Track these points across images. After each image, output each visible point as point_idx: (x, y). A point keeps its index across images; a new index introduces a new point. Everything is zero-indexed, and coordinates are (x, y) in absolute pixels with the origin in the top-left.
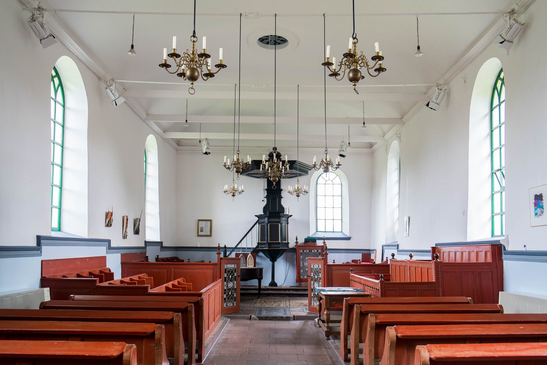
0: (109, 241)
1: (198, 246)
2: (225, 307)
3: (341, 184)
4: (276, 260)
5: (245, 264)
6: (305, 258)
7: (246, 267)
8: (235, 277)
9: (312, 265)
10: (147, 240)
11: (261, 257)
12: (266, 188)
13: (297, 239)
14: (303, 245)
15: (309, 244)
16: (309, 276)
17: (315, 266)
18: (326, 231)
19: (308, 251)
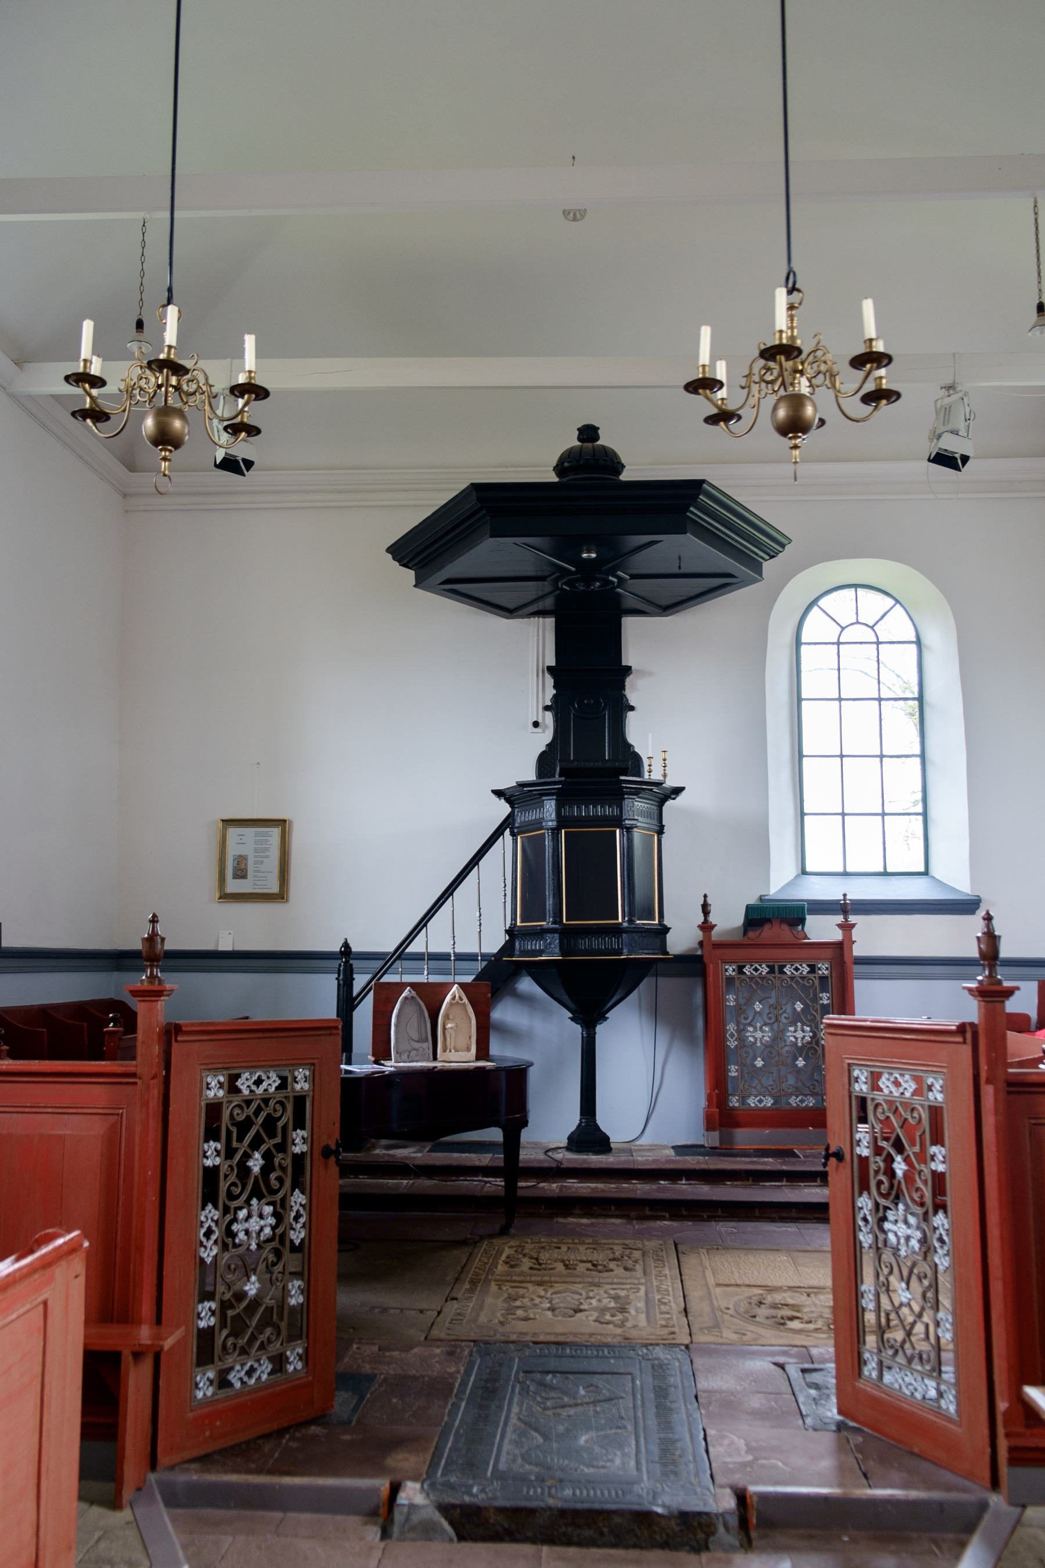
1: (221, 948)
2: (207, 1402)
3: (918, 642)
4: (602, 1017)
5: (425, 1045)
6: (749, 1002)
7: (435, 1058)
8: (298, 1159)
9: (861, 1075)
11: (526, 1000)
12: (551, 661)
13: (705, 909)
14: (738, 938)
15: (767, 933)
16: (839, 1156)
17: (884, 1082)
18: (849, 870)
19: (764, 970)
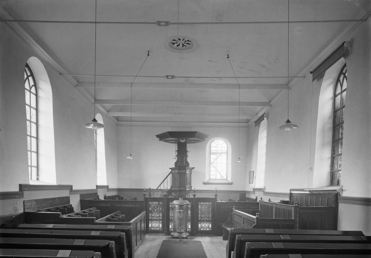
0: (71, 187)
10: (97, 185)
12: (177, 150)
